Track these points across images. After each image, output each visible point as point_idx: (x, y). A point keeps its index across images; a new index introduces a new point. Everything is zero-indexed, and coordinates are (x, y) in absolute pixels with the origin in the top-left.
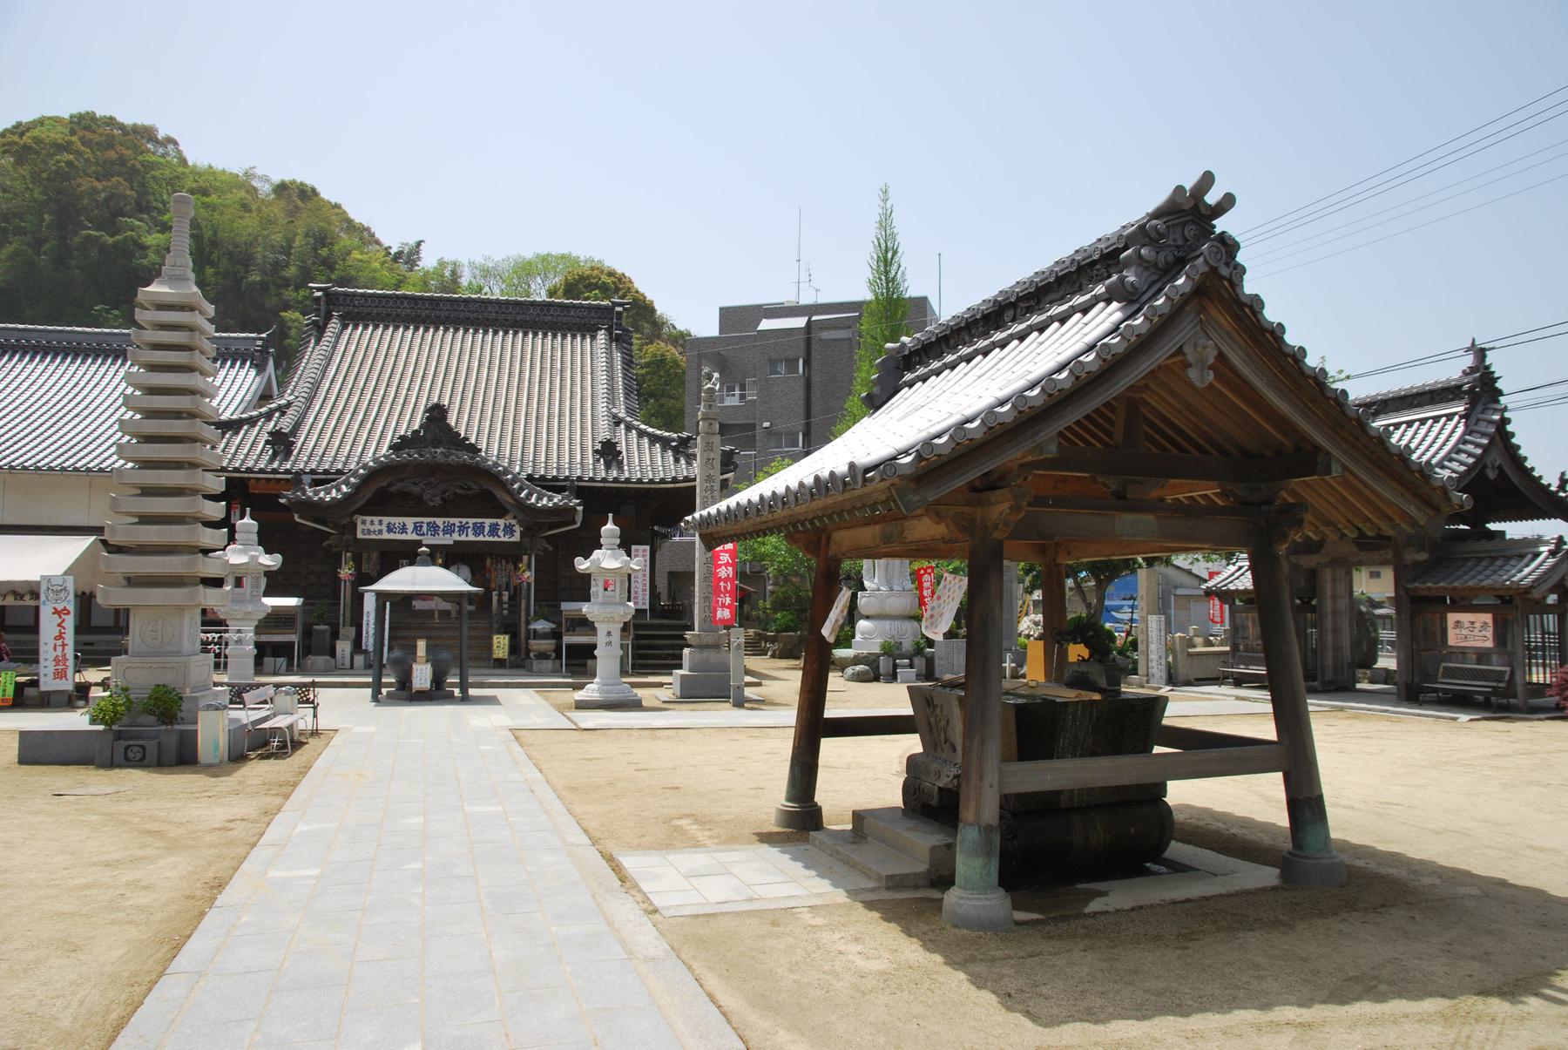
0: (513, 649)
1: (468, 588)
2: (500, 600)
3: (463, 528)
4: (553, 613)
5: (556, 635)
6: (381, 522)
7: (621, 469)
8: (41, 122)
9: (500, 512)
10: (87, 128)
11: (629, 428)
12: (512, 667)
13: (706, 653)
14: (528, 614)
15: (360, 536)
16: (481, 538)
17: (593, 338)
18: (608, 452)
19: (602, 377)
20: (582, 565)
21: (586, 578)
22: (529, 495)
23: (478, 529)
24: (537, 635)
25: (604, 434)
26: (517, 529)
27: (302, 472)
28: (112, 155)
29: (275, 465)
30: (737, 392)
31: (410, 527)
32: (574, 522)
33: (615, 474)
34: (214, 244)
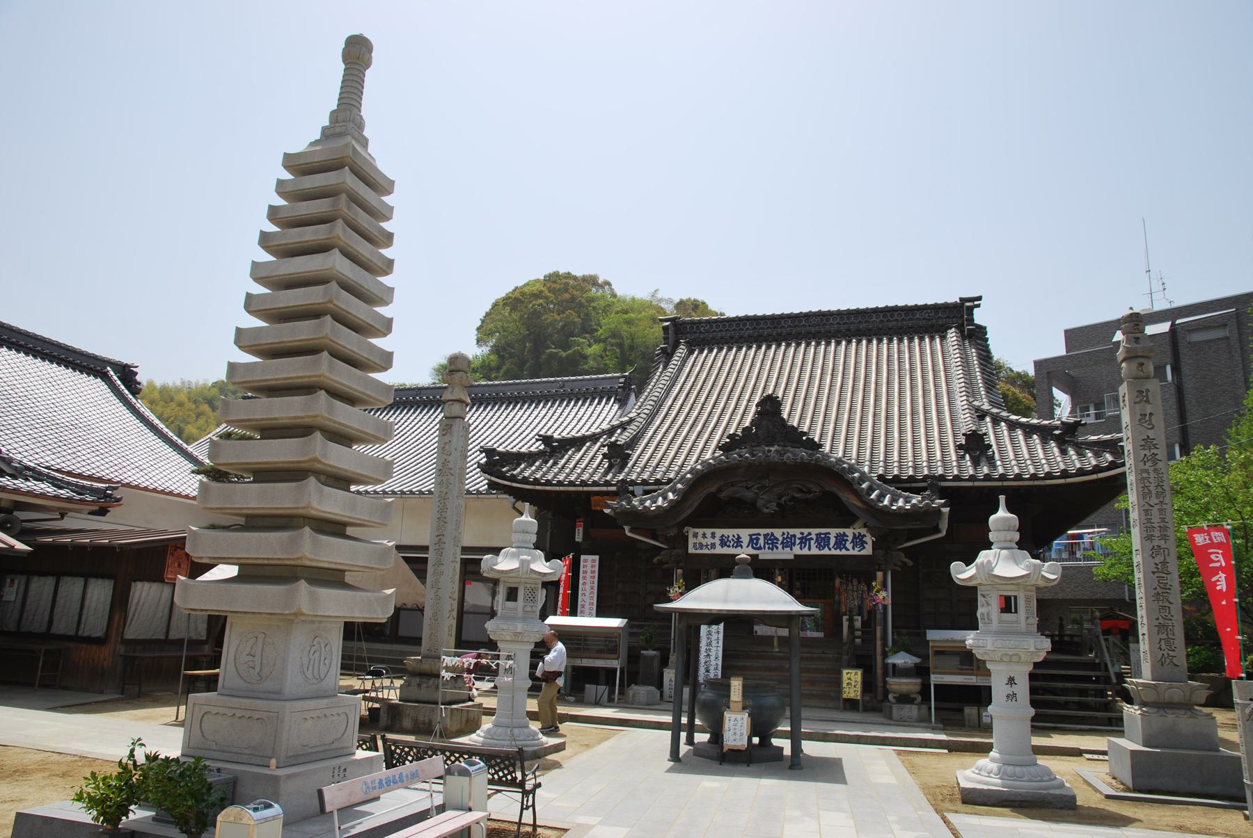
0: (868, 686)
1: (794, 606)
2: (851, 626)
3: (805, 541)
4: (917, 645)
5: (921, 671)
6: (713, 535)
7: (993, 465)
8: (527, 284)
9: (846, 519)
10: (555, 282)
11: (996, 420)
12: (867, 709)
13: (1171, 717)
14: (885, 644)
15: (691, 550)
16: (826, 552)
17: (943, 338)
18: (975, 445)
19: (957, 372)
20: (962, 573)
21: (969, 594)
22: (881, 497)
23: (823, 541)
24: (897, 671)
25: (966, 423)
26: (869, 539)
27: (633, 483)
28: (567, 296)
29: (608, 478)
30: (1092, 412)
31: (745, 540)
32: (937, 530)
33: (986, 470)
34: (632, 348)
